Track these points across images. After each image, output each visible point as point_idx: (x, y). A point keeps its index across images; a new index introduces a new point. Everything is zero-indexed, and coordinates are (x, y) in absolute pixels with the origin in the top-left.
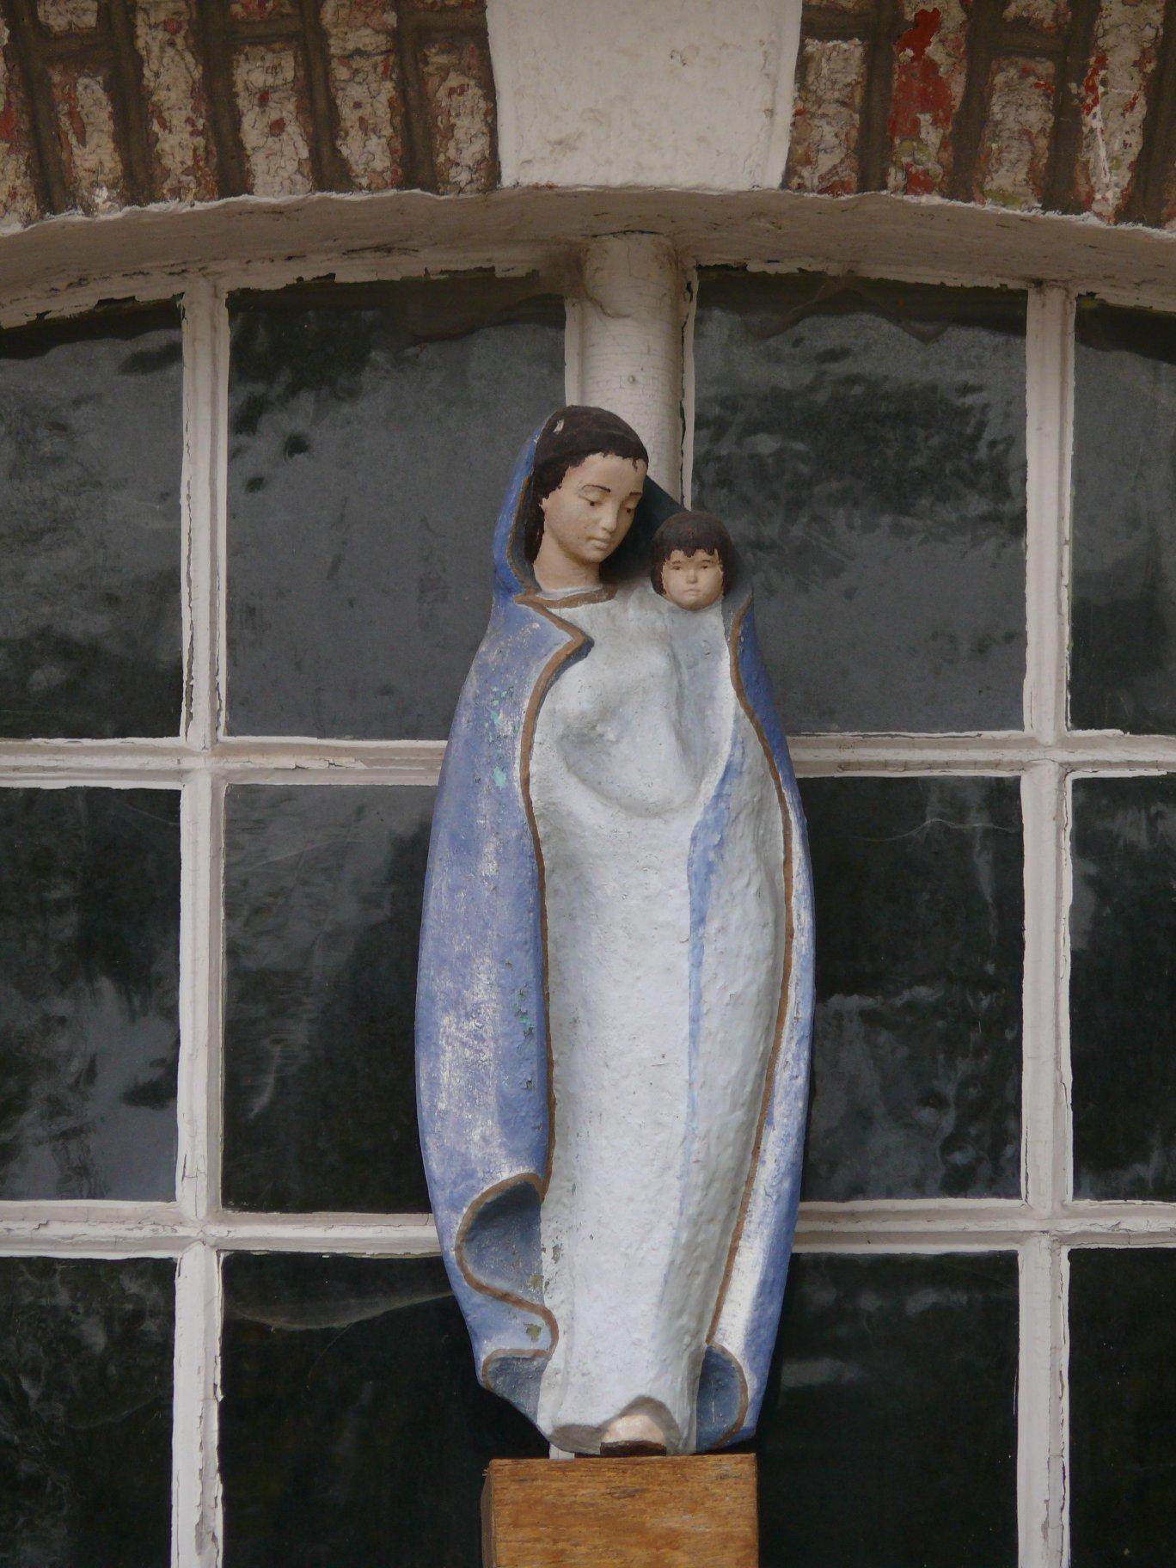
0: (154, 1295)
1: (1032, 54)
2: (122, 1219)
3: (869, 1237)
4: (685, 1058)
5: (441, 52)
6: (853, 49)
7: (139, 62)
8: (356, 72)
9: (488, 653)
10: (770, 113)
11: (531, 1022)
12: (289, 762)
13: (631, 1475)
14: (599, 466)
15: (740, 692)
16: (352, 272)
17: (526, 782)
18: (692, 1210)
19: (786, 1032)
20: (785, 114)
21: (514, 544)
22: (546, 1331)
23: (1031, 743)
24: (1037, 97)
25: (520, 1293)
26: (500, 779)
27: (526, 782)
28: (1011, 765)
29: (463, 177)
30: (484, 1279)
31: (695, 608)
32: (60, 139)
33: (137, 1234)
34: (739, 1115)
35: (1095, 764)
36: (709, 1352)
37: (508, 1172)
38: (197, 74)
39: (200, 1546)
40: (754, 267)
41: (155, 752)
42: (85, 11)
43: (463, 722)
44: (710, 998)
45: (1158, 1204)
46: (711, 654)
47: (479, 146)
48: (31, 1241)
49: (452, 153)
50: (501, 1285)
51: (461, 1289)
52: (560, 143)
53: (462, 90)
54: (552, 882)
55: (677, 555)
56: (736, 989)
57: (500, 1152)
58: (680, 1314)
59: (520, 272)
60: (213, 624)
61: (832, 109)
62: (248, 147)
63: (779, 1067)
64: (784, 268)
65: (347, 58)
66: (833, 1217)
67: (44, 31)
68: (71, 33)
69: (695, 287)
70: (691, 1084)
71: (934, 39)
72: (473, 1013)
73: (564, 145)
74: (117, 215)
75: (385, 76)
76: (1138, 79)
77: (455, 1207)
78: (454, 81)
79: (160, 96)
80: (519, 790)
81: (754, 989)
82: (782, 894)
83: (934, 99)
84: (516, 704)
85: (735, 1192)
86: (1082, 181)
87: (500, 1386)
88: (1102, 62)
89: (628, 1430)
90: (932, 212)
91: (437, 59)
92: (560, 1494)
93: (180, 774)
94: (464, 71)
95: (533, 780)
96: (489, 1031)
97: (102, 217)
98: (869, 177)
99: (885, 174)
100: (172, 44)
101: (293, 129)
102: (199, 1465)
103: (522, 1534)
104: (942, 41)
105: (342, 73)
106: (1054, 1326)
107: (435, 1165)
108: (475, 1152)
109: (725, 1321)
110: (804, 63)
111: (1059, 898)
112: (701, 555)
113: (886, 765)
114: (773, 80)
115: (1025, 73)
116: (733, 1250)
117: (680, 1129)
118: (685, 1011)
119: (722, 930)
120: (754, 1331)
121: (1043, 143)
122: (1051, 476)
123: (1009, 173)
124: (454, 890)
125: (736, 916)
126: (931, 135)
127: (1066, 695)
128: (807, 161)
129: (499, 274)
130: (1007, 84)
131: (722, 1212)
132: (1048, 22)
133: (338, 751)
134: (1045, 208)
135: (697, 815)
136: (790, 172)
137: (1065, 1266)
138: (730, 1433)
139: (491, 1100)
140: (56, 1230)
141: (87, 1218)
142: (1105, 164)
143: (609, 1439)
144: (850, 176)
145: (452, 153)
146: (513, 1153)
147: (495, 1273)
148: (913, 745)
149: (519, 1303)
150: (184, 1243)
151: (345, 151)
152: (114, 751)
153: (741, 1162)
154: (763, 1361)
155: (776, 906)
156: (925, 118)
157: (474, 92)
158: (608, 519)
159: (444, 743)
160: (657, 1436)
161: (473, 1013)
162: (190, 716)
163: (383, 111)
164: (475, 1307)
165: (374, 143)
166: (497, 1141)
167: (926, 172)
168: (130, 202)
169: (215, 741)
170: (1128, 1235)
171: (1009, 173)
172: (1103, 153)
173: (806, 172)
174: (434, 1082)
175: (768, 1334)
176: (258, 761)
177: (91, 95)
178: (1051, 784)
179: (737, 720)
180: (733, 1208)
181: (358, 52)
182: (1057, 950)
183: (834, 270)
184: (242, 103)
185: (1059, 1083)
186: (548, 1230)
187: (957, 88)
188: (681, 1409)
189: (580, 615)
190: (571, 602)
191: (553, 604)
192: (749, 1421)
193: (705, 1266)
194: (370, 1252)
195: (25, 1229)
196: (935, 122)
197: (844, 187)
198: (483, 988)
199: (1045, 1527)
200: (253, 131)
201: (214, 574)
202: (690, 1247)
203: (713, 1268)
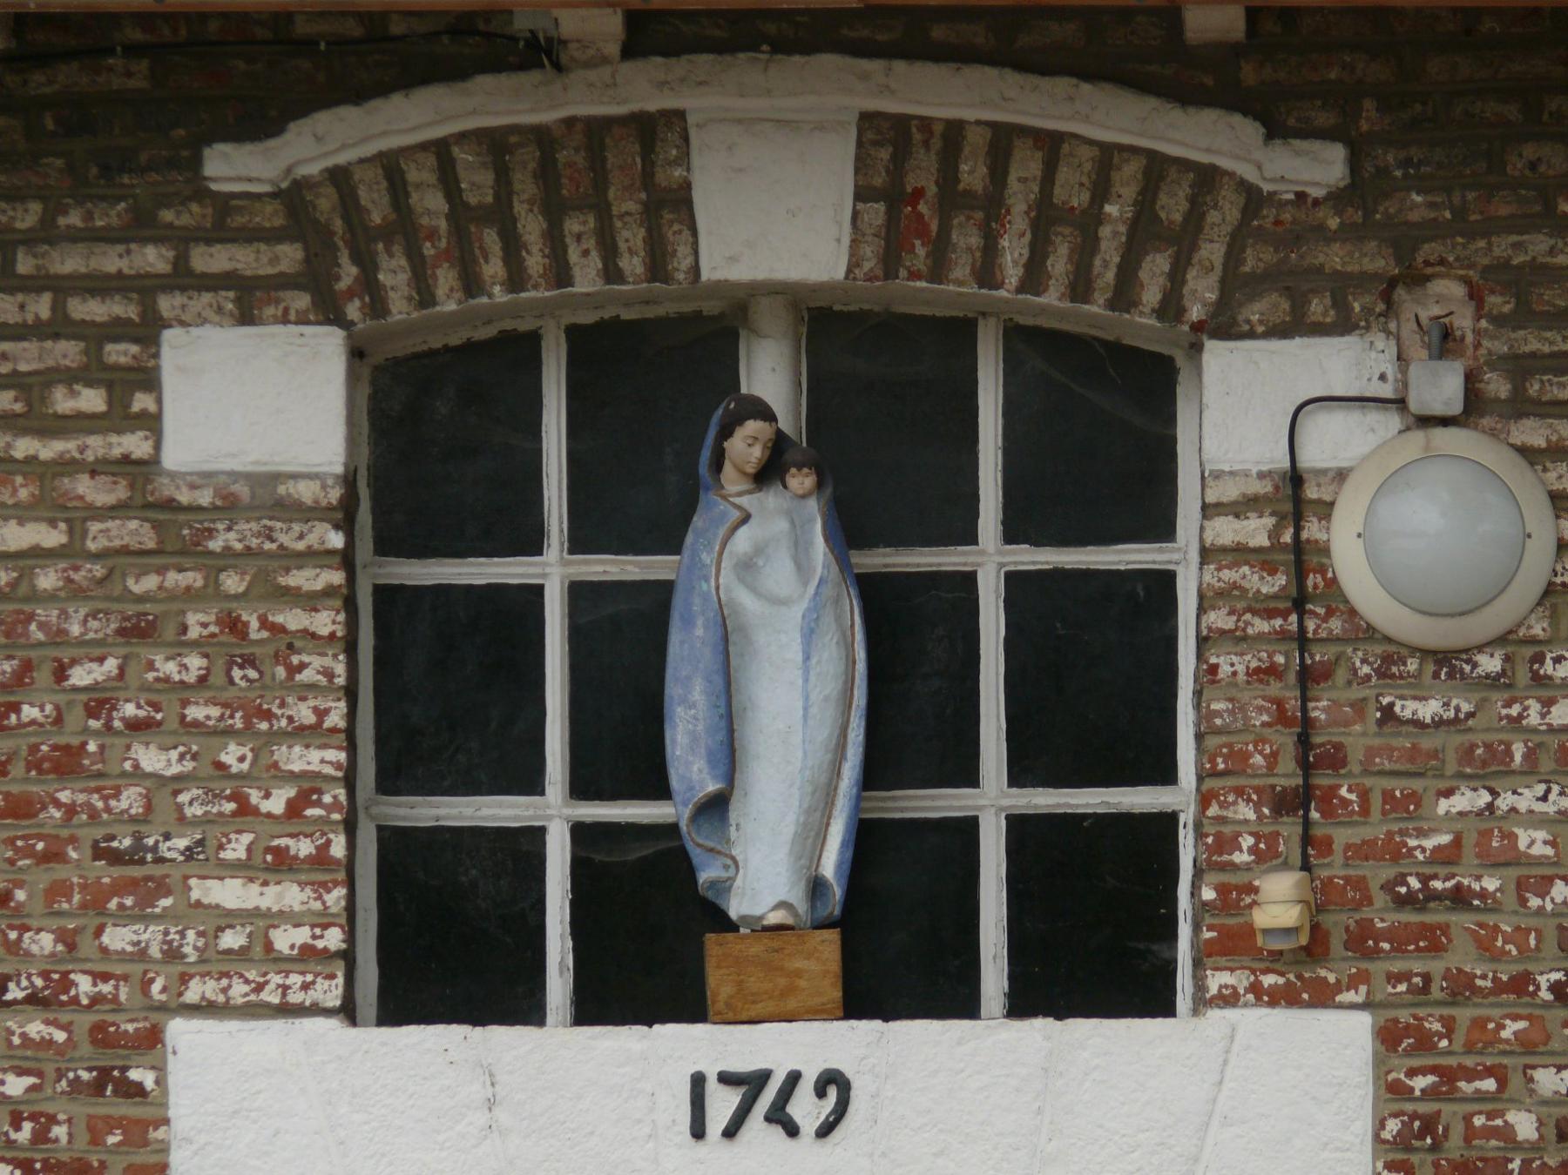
0: (579, 126)
1: (972, 208)
2: (518, 806)
3: (902, 810)
4: (800, 728)
5: (670, 212)
6: (881, 207)
7: (514, 220)
8: (625, 223)
9: (698, 521)
10: (838, 241)
11: (722, 710)
12: (600, 569)
13: (775, 941)
14: (752, 427)
15: (826, 540)
16: (627, 315)
17: (717, 588)
18: (806, 806)
19: (853, 714)
20: (846, 241)
21: (710, 466)
22: (733, 867)
23: (983, 553)
24: (975, 231)
25: (719, 847)
26: (705, 586)
27: (717, 588)
28: (973, 564)
29: (681, 276)
30: (701, 841)
31: (803, 497)
32: (475, 261)
33: (526, 813)
34: (829, 756)
35: (1015, 563)
36: (816, 877)
37: (712, 787)
38: (545, 226)
39: (561, 973)
40: (837, 308)
41: (531, 564)
42: (487, 194)
43: (686, 551)
44: (813, 697)
45: (1051, 790)
46: (812, 520)
47: (689, 261)
48: (472, 818)
49: (675, 264)
50: (710, 844)
51: (690, 846)
52: (730, 258)
53: (680, 232)
54: (732, 638)
55: (793, 470)
56: (827, 692)
57: (708, 777)
58: (800, 859)
59: (716, 312)
60: (560, 497)
61: (870, 238)
62: (571, 263)
63: (850, 730)
64: (852, 308)
65: (621, 216)
66: (884, 799)
67: (466, 205)
68: (481, 206)
69: (806, 319)
70: (804, 742)
71: (921, 202)
72: (693, 706)
73: (733, 259)
74: (505, 299)
75: (641, 225)
76: (1027, 221)
77: (686, 805)
78: (676, 227)
79: (526, 238)
80: (714, 592)
81: (835, 693)
82: (850, 639)
83: (922, 231)
84: (712, 549)
85: (828, 794)
86: (998, 273)
87: (710, 895)
88: (1008, 212)
89: (774, 918)
90: (923, 290)
91: (667, 216)
92: (741, 951)
93: (544, 576)
94: (681, 223)
95: (721, 587)
96: (701, 715)
97: (498, 300)
98: (890, 273)
99: (897, 271)
100: (531, 211)
101: (594, 253)
102: (560, 931)
103: (722, 971)
104: (926, 203)
105: (619, 224)
106: (998, 853)
107: (675, 783)
108: (695, 777)
109: (824, 860)
110: (855, 215)
111: (998, 632)
112: (806, 470)
113: (908, 565)
114: (839, 224)
115: (969, 218)
116: (828, 824)
117: (799, 765)
118: (800, 704)
119: (819, 662)
120: (839, 866)
121: (978, 254)
122: (992, 407)
123: (961, 269)
124: (682, 643)
125: (826, 655)
126: (921, 251)
127: (1000, 527)
128: (858, 265)
129: (705, 313)
130: (960, 224)
131: (822, 805)
132: (980, 191)
133: (624, 562)
134: (980, 288)
135: (804, 604)
136: (849, 271)
137: (1004, 822)
138: (828, 917)
139: (703, 750)
140: (485, 812)
141: (500, 806)
142: (1010, 264)
143: (765, 923)
144: (879, 272)
145: (675, 264)
146: (715, 778)
147: (707, 838)
148: (921, 554)
149: (719, 853)
150: (550, 818)
151: (621, 264)
152: (510, 564)
153: (831, 780)
154: (844, 881)
155: (847, 649)
156: (918, 243)
157: (687, 233)
158: (757, 453)
159: (677, 558)
160: (790, 921)
161: (693, 706)
162: (549, 546)
163: (640, 243)
164: (696, 854)
165: (636, 261)
166: (706, 771)
167: (919, 270)
168: (511, 292)
169: (562, 558)
170: (1036, 806)
171: (961, 269)
172: (1009, 258)
173: (857, 271)
174: (674, 741)
175: (847, 867)
176: (584, 569)
177: (491, 238)
178: (993, 574)
179: (825, 555)
180: (827, 803)
181: (628, 213)
182: (997, 659)
183: (876, 309)
184: (568, 240)
185: (999, 727)
186: (733, 815)
187: (934, 227)
188: (802, 907)
189: (744, 501)
190: (740, 494)
191: (730, 496)
192: (837, 912)
193: (812, 834)
194: (645, 821)
195: (469, 811)
196: (923, 244)
197: (877, 278)
198: (698, 693)
199: (994, 958)
200: (573, 255)
201: (560, 472)
202: (805, 824)
203: (818, 834)
